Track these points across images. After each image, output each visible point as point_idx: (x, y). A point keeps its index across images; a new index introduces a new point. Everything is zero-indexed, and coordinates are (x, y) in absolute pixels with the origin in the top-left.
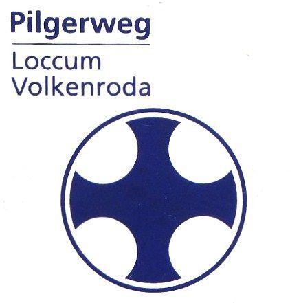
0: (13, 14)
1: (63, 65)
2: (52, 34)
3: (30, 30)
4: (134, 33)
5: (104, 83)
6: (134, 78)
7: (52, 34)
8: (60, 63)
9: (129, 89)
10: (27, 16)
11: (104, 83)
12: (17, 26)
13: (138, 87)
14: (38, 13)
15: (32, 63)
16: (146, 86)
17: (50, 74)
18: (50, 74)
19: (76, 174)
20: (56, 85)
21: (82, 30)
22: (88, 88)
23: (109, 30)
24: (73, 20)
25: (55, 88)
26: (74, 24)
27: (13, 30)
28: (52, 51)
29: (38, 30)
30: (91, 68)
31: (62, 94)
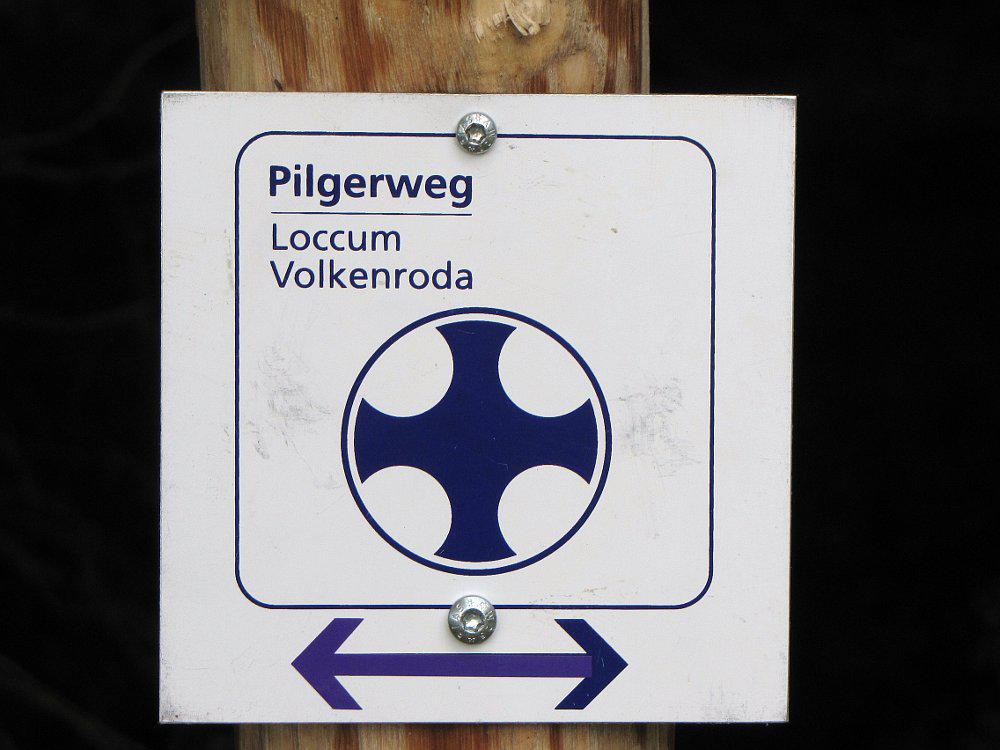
0: (274, 169)
3: (297, 193)
4: (449, 198)
5: (405, 270)
6: (449, 263)
9: (442, 279)
10: (293, 172)
11: (405, 270)
13: (455, 276)
14: (310, 168)
15: (300, 240)
17: (327, 256)
18: (327, 256)
20: (335, 273)
21: (374, 194)
22: (381, 277)
24: (360, 178)
25: (334, 277)
26: (362, 184)
27: (273, 192)
28: (330, 223)
29: (310, 193)
31: (343, 286)
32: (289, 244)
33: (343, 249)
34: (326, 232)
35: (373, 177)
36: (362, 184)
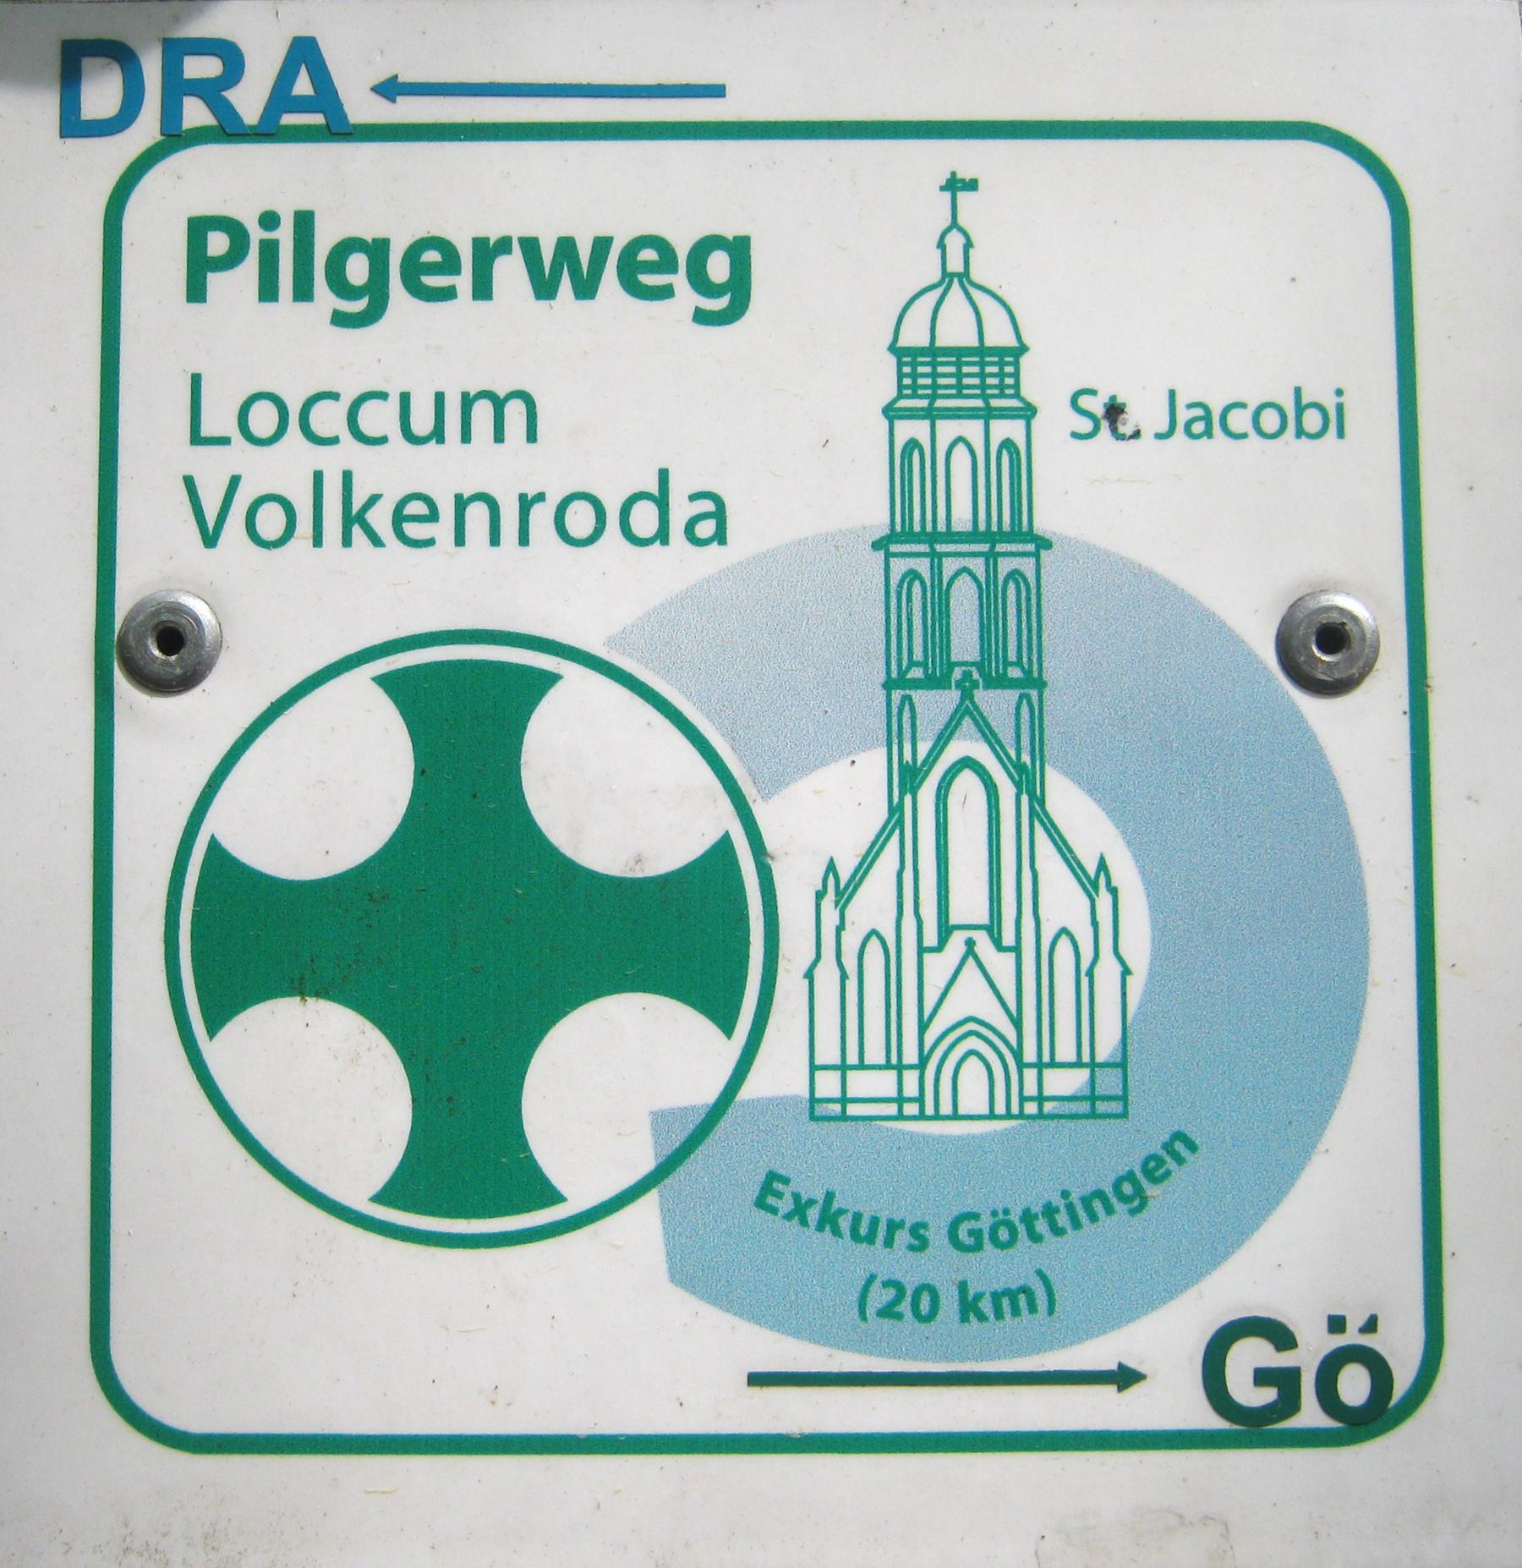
1: (393, 430)
2: (359, 306)
3: (268, 291)
4: (686, 298)
5: (541, 497)
6: (663, 475)
7: (358, 306)
8: (379, 418)
10: (256, 234)
11: (541, 497)
12: (215, 280)
13: (681, 512)
14: (304, 222)
15: (263, 419)
16: (708, 506)
17: (331, 462)
18: (331, 462)
19: (378, 1198)
20: (357, 504)
21: (483, 289)
22: (477, 515)
23: (586, 289)
24: (446, 248)
25: (354, 519)
26: (451, 263)
27: (196, 292)
29: (303, 292)
30: (757, 1380)
31: (376, 541)
32: (233, 431)
33: (383, 440)
34: (335, 396)
35: (480, 245)
36: (451, 263)
